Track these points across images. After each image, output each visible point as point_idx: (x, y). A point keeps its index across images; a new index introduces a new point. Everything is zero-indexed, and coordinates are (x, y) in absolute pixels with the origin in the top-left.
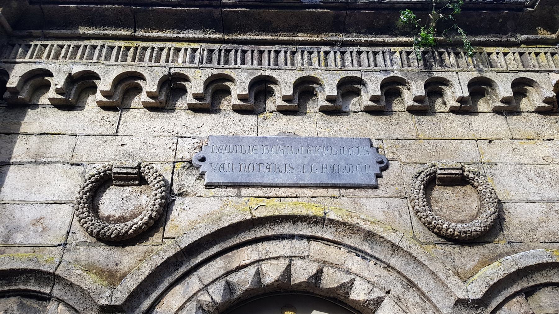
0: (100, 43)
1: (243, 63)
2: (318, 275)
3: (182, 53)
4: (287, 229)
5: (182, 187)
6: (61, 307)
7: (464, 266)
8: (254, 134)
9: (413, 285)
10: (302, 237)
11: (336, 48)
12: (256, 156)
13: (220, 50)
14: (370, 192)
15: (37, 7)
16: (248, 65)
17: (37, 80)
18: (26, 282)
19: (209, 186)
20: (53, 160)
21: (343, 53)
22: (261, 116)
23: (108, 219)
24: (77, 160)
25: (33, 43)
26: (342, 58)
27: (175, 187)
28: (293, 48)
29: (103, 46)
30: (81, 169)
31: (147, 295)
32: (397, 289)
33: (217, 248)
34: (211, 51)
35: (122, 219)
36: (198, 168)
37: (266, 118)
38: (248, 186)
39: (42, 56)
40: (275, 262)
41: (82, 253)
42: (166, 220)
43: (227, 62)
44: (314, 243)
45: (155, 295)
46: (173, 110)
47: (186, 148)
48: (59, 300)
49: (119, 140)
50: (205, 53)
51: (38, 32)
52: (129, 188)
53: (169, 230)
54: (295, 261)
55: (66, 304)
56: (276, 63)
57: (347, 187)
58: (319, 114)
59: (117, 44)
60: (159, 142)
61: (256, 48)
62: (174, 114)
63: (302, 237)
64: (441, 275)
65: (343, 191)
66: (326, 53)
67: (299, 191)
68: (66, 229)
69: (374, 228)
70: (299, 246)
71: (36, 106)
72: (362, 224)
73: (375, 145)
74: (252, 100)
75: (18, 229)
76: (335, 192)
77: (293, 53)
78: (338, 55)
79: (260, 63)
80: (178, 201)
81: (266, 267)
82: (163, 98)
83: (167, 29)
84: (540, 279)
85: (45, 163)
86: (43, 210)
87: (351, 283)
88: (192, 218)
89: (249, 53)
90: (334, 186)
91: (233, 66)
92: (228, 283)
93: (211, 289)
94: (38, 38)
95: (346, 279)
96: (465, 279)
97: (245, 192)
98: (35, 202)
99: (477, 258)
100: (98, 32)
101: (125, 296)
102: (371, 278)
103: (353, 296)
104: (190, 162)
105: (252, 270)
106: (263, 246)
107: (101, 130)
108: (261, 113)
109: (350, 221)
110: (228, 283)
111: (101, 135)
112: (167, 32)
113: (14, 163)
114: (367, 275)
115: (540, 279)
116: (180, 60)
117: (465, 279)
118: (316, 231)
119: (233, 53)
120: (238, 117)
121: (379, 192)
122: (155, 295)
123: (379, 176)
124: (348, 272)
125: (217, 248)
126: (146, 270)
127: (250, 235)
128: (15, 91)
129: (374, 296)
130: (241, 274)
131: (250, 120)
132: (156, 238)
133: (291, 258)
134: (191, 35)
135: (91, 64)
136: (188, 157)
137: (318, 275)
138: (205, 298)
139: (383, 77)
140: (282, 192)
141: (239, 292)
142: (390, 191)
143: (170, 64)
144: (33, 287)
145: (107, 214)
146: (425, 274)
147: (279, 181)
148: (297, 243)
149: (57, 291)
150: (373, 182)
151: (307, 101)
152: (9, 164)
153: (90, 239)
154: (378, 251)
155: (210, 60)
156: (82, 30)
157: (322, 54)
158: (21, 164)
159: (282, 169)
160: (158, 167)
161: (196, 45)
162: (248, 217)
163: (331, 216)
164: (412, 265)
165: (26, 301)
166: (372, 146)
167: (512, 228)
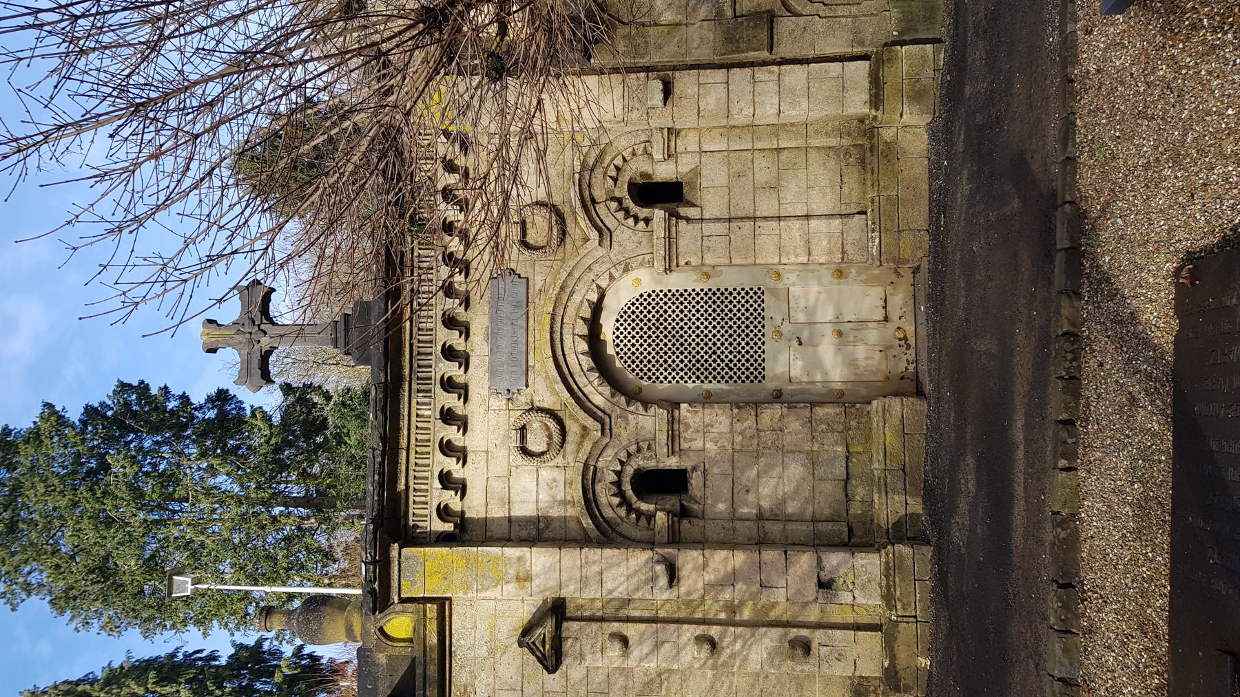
0: (411, 473)
2: (584, 319)
4: (557, 336)
5: (527, 403)
8: (487, 358)
10: (561, 328)
12: (506, 356)
14: (531, 283)
15: (385, 521)
17: (443, 513)
22: (471, 353)
23: (549, 445)
24: (506, 473)
25: (411, 523)
28: (415, 330)
30: (513, 469)
32: (592, 276)
33: (571, 380)
34: (418, 391)
35: (550, 436)
37: (472, 350)
38: (527, 362)
39: (144, 661)
41: (570, 458)
44: (565, 321)
45: (595, 410)
46: (466, 416)
47: (498, 403)
48: (597, 461)
49: (492, 448)
50: (420, 395)
53: (557, 407)
54: (576, 332)
57: (528, 298)
58: (468, 312)
59: (412, 461)
62: (469, 415)
63: (561, 328)
64: (586, 251)
67: (531, 328)
68: (555, 469)
77: (419, 329)
80: (537, 404)
81: (579, 349)
82: (459, 423)
83: (399, 424)
86: (543, 485)
87: (588, 300)
88: (549, 394)
89: (420, 362)
91: (433, 374)
94: (407, 519)
97: (531, 363)
98: (537, 492)
100: (403, 474)
103: (595, 300)
105: (581, 357)
106: (567, 352)
107: (483, 462)
111: (487, 462)
112: (600, 389)
114: (584, 292)
115: (587, 194)
116: (427, 413)
121: (531, 277)
122: (595, 410)
124: (582, 302)
126: (582, 415)
127: (561, 358)
128: (456, 526)
130: (583, 363)
131: (473, 361)
132: (561, 414)
133: (574, 335)
135: (432, 474)
136: (505, 402)
137: (584, 319)
140: (531, 339)
142: (530, 270)
146: (584, 260)
147: (524, 341)
149: (592, 463)
150: (525, 280)
151: (457, 321)
152: (510, 517)
153: (561, 453)
154: (571, 284)
156: (401, 487)
158: (509, 509)
161: (414, 402)
163: (551, 310)
164: (579, 266)
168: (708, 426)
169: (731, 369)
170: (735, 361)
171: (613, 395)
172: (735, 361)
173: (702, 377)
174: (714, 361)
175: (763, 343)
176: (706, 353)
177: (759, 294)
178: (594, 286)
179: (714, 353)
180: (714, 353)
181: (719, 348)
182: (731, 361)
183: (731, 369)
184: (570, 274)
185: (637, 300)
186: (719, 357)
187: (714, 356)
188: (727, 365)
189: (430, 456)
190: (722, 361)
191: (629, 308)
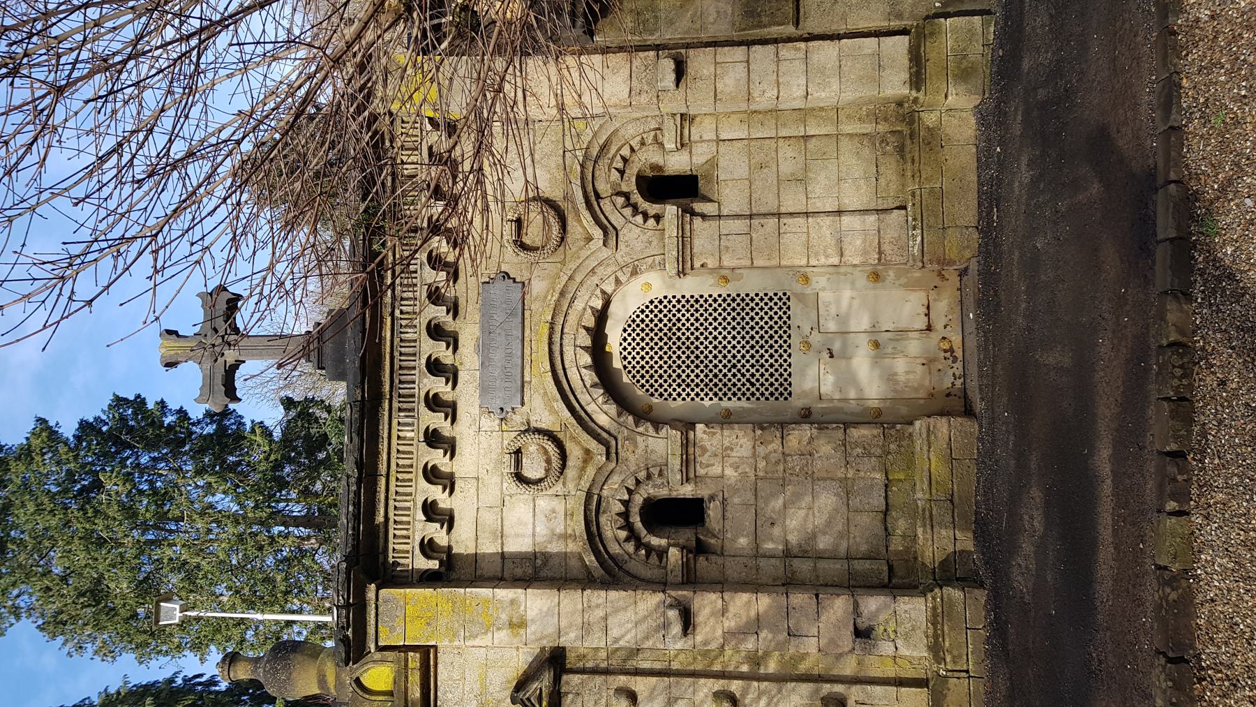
1: (414, 382)
3: (401, 434)
4: (556, 348)
6: (605, 487)
7: (579, 233)
8: (478, 373)
9: (593, 269)
10: (561, 338)
11: (397, 304)
12: (499, 370)
13: (400, 402)
16: (416, 378)
18: (591, 511)
19: (523, 404)
20: (499, 520)
21: (402, 299)
22: (459, 368)
24: (499, 503)
25: (391, 560)
26: (407, 299)
27: (522, 429)
28: (397, 341)
29: (395, 500)
30: (507, 498)
31: (599, 435)
33: (572, 398)
34: (400, 410)
35: (548, 461)
36: (507, 412)
37: (461, 364)
40: (578, 356)
42: (548, 431)
43: (413, 396)
44: (565, 330)
45: (599, 431)
48: (601, 489)
50: (402, 414)
51: (381, 557)
52: (524, 460)
54: (578, 343)
55: (604, 484)
56: (414, 355)
60: (484, 445)
61: (397, 372)
62: (458, 437)
64: (589, 253)
65: (526, 307)
66: (402, 312)
67: (527, 339)
69: (558, 290)
70: (567, 340)
71: (450, 548)
72: (554, 298)
73: (487, 280)
74: (447, 375)
75: (553, 531)
76: (527, 314)
78: (403, 303)
79: (414, 368)
80: (533, 424)
82: (446, 446)
84: (590, 188)
85: (502, 526)
86: (540, 517)
87: (592, 308)
88: (547, 413)
90: (523, 314)
91: (417, 390)
92: (592, 386)
93: (595, 396)
94: (386, 556)
95: (589, 311)
96: (589, 239)
97: (527, 378)
99: (575, 224)
101: (601, 446)
102: (589, 294)
104: (502, 419)
105: (584, 371)
107: (473, 491)
108: (456, 367)
109: (552, 306)
110: (592, 386)
111: (477, 490)
112: (605, 407)
113: (502, 549)
114: (587, 298)
115: (590, 188)
117: (589, 239)
118: (558, 328)
119: (401, 391)
120: (459, 385)
122: (599, 431)
123: (514, 280)
125: (572, 398)
127: (561, 372)
129: (600, 295)
130: (586, 378)
131: (462, 376)
132: (560, 436)
133: (575, 346)
134: (386, 426)
136: (497, 422)
138: (600, 400)
139: (427, 268)
140: (527, 351)
141: (597, 380)
143: (415, 442)
144: (593, 507)
145: (543, 472)
147: (519, 354)
148: (565, 342)
149: (596, 491)
150: (520, 285)
151: (444, 330)
153: (561, 480)
154: (572, 289)
155: (412, 410)
156: (380, 518)
157: (403, 316)
158: (502, 544)
159: (510, 351)
160: (506, 442)
161: (395, 422)
162: (550, 374)
164: (581, 268)
165: (602, 509)
166: (488, 283)
167: (554, 194)
168: (727, 448)
169: (753, 385)
170: (758, 375)
171: (619, 415)
172: (758, 375)
173: (720, 394)
174: (734, 375)
175: (790, 356)
176: (725, 366)
177: (784, 299)
178: (598, 292)
179: (734, 366)
180: (734, 366)
181: (739, 361)
182: (753, 375)
183: (753, 385)
184: (571, 278)
185: (647, 307)
186: (739, 371)
187: (734, 370)
188: (748, 380)
189: (413, 484)
190: (743, 375)
191: (638, 316)
